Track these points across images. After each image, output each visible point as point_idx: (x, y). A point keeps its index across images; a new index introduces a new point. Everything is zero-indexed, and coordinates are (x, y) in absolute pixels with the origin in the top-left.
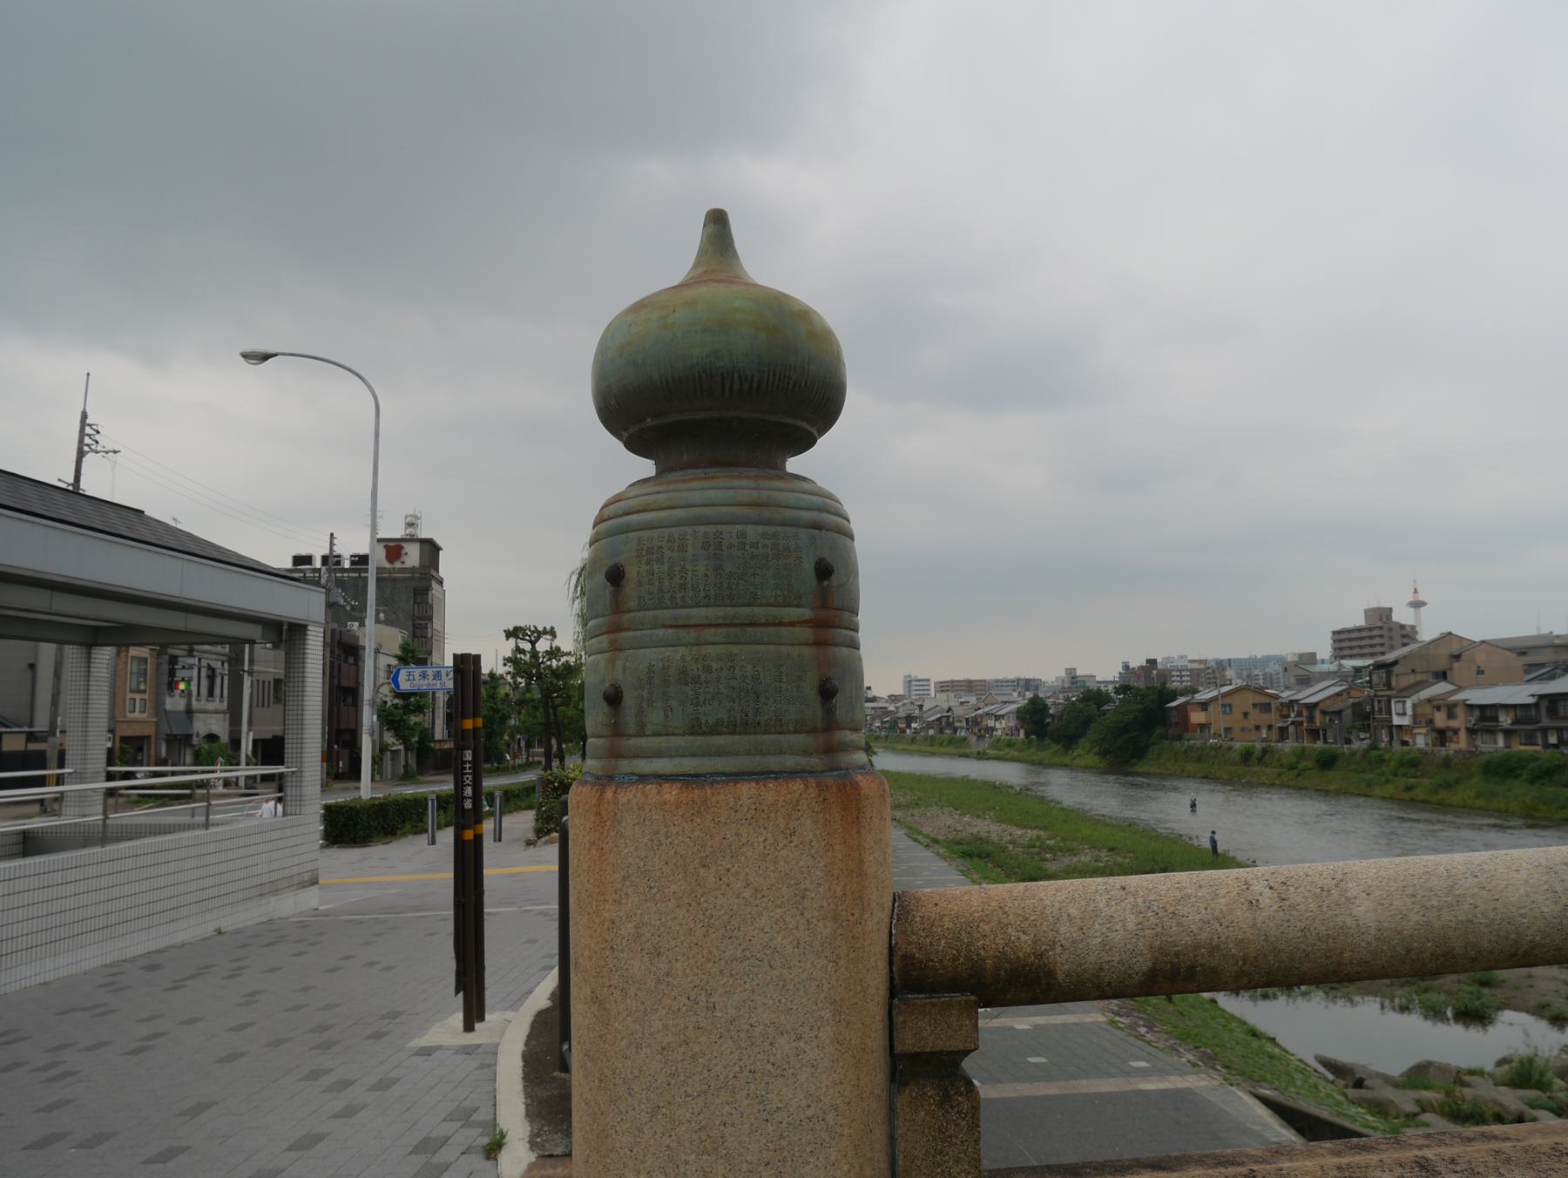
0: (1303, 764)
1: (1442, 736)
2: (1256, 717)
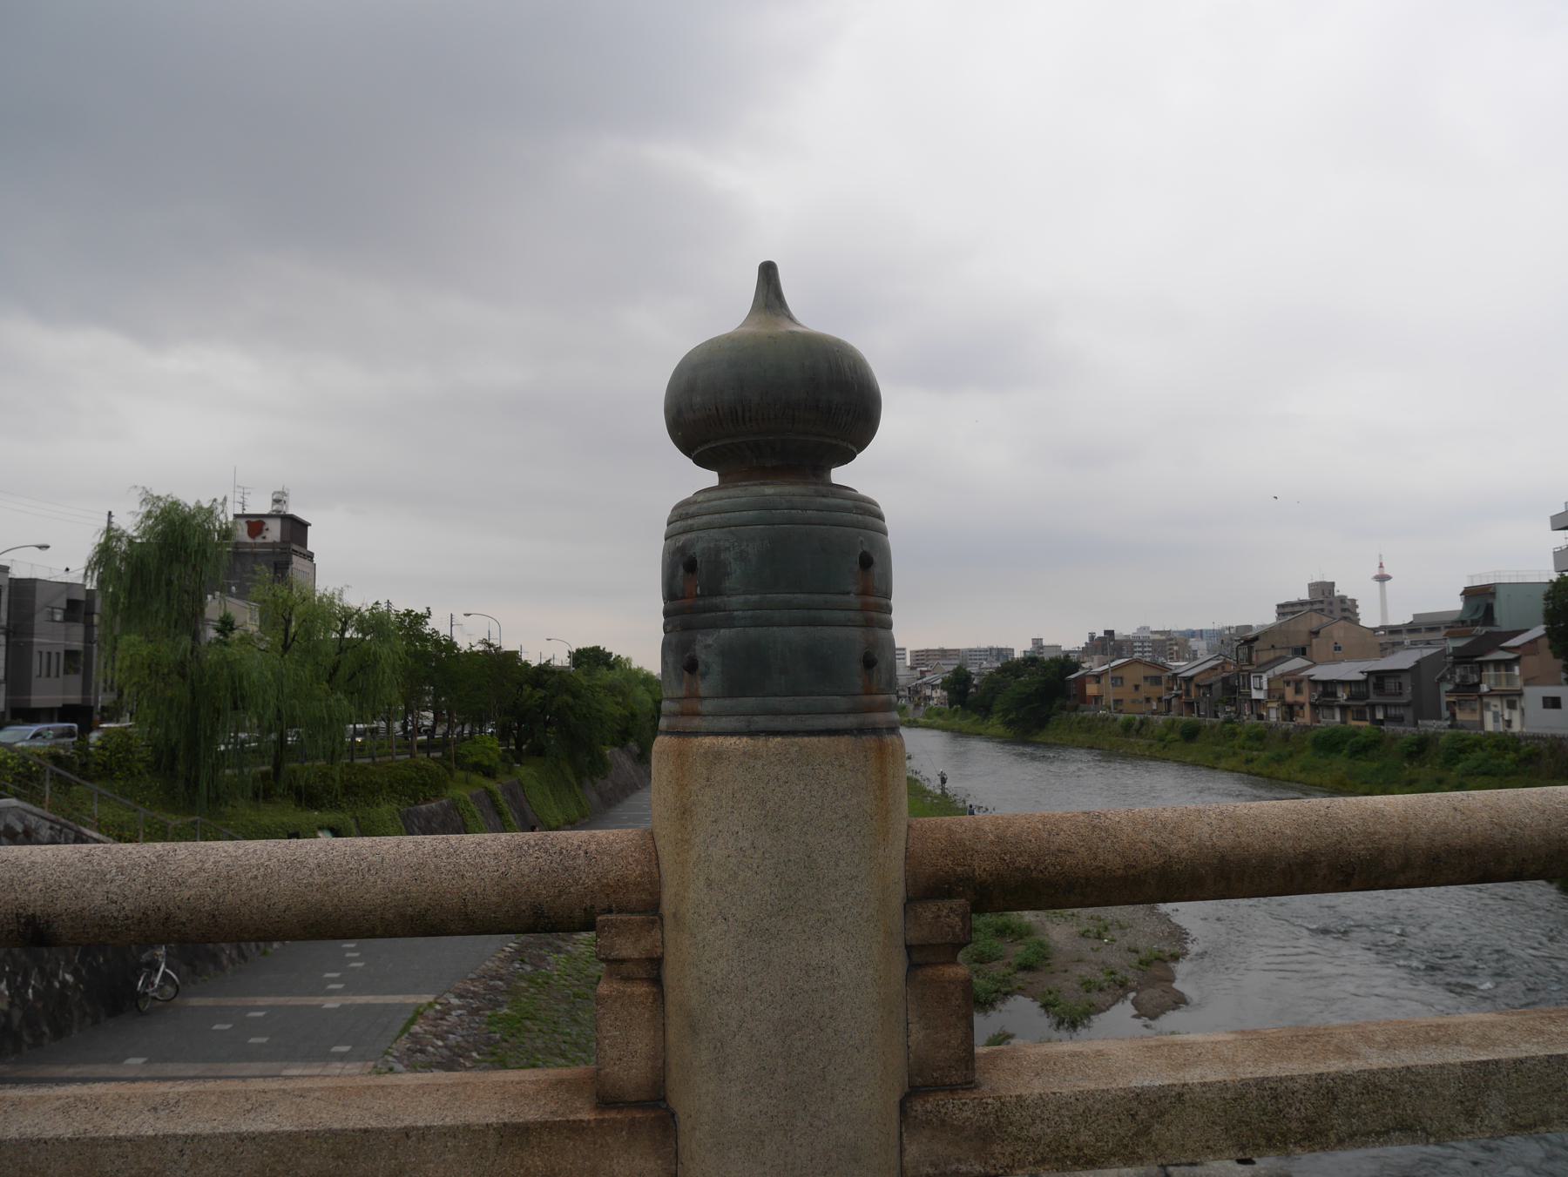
0: (1171, 736)
1: (1290, 710)
2: (1147, 689)
